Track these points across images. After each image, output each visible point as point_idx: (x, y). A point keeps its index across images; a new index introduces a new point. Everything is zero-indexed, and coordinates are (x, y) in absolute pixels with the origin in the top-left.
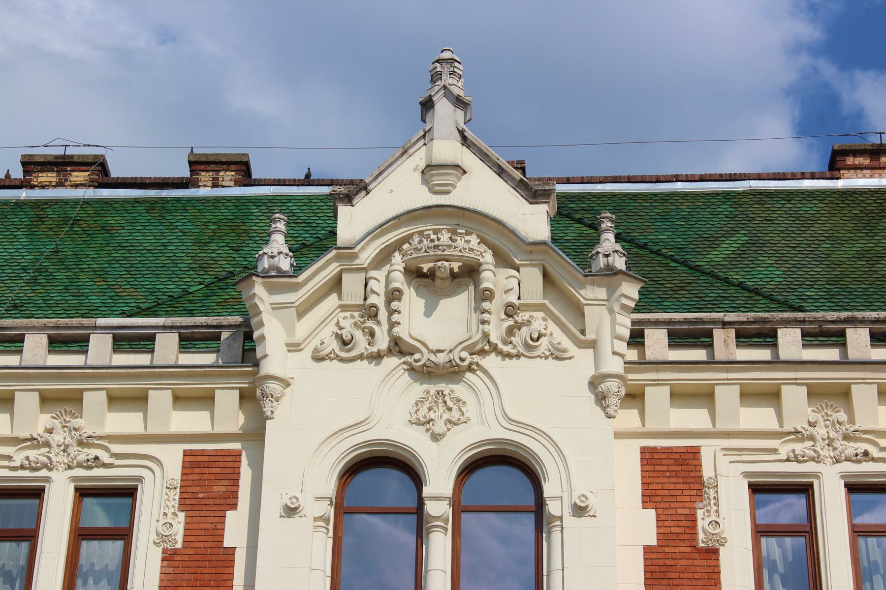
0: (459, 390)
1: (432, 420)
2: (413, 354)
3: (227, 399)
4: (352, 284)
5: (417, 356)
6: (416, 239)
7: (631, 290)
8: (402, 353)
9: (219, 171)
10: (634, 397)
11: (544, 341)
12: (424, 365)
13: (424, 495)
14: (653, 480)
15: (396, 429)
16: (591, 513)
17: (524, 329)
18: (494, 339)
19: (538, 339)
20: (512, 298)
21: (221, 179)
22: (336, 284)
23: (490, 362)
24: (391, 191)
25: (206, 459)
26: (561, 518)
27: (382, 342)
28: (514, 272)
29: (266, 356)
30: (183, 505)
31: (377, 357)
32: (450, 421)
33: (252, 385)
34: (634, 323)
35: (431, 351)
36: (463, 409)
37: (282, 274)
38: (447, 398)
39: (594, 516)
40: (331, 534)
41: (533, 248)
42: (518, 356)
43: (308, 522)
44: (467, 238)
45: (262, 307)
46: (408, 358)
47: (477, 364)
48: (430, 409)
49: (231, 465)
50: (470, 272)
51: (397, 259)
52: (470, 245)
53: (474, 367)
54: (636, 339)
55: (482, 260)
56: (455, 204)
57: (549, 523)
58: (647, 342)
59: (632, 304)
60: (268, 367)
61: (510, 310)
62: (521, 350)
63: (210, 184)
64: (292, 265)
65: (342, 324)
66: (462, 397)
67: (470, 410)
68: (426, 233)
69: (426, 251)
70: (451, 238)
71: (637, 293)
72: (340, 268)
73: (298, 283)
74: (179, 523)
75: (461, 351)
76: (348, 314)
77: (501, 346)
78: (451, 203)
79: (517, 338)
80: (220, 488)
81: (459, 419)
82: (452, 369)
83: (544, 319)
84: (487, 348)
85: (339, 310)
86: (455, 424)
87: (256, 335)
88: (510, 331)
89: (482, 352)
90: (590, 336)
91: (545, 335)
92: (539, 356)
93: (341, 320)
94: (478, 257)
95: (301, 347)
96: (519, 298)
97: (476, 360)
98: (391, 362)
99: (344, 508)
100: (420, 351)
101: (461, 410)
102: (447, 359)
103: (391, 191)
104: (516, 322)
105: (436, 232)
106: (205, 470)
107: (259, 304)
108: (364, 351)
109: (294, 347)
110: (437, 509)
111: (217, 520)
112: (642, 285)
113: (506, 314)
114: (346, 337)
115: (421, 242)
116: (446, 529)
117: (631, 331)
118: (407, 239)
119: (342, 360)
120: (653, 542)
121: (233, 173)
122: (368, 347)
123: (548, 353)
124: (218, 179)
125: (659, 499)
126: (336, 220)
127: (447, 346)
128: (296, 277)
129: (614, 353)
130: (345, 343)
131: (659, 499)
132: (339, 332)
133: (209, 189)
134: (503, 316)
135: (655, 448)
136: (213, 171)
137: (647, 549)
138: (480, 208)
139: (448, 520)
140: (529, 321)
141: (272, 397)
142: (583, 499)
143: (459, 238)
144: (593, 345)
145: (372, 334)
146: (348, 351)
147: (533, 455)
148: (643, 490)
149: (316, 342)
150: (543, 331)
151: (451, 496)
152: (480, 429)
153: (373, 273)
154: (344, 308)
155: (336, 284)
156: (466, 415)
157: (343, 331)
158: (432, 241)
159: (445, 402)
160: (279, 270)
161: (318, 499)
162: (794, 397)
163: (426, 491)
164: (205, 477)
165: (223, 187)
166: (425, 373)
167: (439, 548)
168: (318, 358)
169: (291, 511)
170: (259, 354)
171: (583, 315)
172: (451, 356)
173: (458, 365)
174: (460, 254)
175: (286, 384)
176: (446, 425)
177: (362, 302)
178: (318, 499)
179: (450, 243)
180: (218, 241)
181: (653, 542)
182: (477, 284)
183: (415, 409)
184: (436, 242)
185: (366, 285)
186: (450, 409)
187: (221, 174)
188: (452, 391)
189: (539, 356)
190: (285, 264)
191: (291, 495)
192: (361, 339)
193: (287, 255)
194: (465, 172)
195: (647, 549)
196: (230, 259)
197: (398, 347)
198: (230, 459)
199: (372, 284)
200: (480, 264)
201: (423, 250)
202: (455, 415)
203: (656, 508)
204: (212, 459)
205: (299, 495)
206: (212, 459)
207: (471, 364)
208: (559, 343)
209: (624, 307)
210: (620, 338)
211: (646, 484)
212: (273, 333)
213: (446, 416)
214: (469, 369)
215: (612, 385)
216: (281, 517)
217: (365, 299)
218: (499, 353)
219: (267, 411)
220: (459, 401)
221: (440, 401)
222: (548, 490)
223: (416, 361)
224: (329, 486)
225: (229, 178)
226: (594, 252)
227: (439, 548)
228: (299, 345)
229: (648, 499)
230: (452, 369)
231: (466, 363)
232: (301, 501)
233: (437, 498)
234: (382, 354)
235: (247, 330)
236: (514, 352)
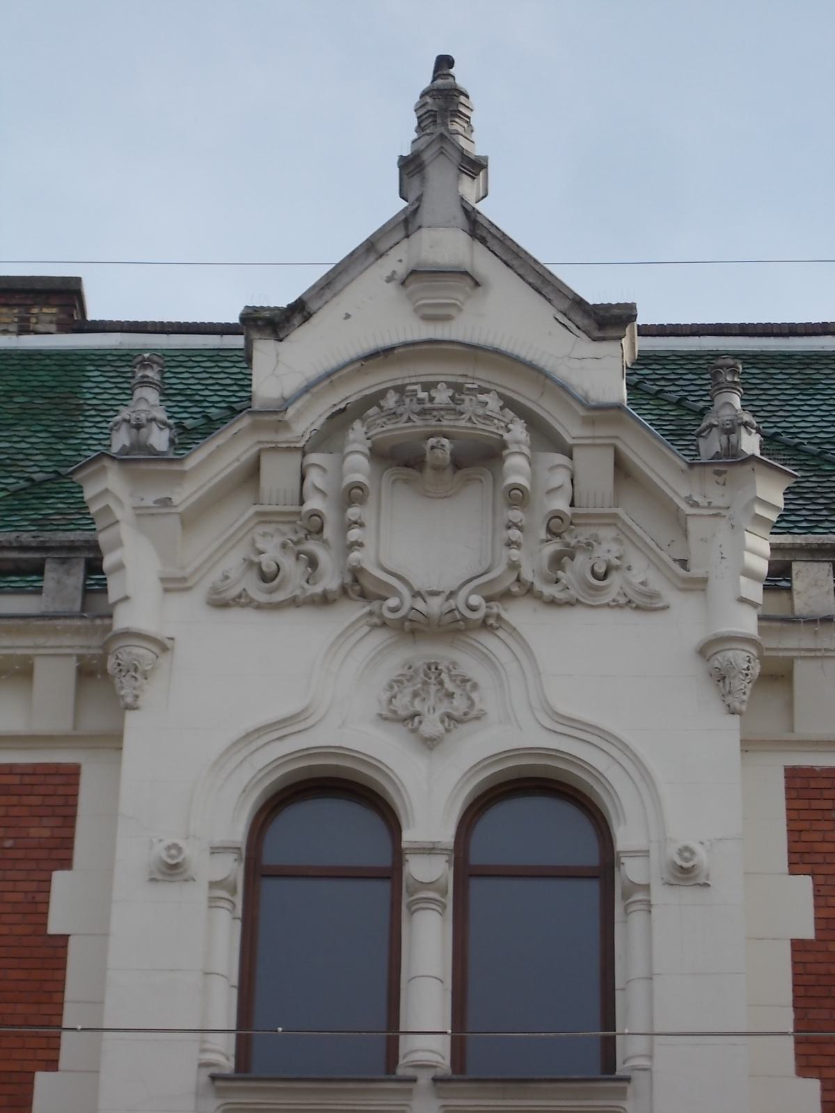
0: (468, 664)
1: (417, 714)
2: (386, 599)
3: (55, 676)
4: (278, 476)
5: (393, 602)
6: (391, 401)
7: (771, 492)
8: (364, 595)
9: (32, 306)
10: (777, 676)
11: (615, 579)
12: (404, 618)
13: (404, 845)
14: (805, 825)
15: (351, 728)
16: (701, 881)
17: (580, 558)
18: (527, 575)
19: (605, 576)
20: (560, 504)
21: (33, 320)
22: (253, 472)
23: (519, 614)
24: (348, 316)
25: (16, 780)
26: (646, 888)
27: (330, 581)
28: (561, 459)
29: (126, 599)
31: (325, 600)
32: (449, 716)
33: (100, 652)
34: (775, 548)
35: (416, 594)
36: (475, 696)
37: (156, 457)
38: (444, 676)
39: (707, 885)
40: (239, 912)
41: (597, 413)
42: (570, 604)
43: (198, 893)
44: (483, 398)
45: (119, 514)
46: (375, 606)
47: (499, 617)
48: (415, 695)
49: (61, 790)
50: (481, 457)
51: (357, 435)
52: (484, 415)
53: (491, 621)
54: (779, 577)
55: (506, 436)
56: (460, 339)
57: (626, 896)
58: (797, 584)
59: (774, 517)
60: (124, 619)
61: (556, 526)
62: (574, 593)
63: (13, 328)
64: (172, 442)
65: (260, 546)
66: (470, 675)
67: (487, 699)
68: (409, 388)
69: (409, 420)
70: (452, 398)
71: (782, 497)
72: (256, 449)
73: (185, 472)
75: (473, 592)
76: (269, 528)
77: (539, 586)
78: (453, 337)
79: (569, 574)
80: (39, 832)
81: (466, 714)
82: (454, 626)
83: (617, 540)
84: (515, 589)
85: (256, 520)
86: (459, 721)
87: (108, 563)
88: (557, 561)
89: (507, 595)
90: (696, 572)
91: (617, 568)
92: (608, 605)
93: (258, 539)
94: (500, 432)
95: (189, 584)
96: (572, 505)
97: (495, 610)
98: (354, 611)
99: (257, 869)
100: (396, 592)
101: (469, 698)
102: (446, 608)
103: (348, 316)
104: (568, 545)
105: (427, 387)
106: (15, 800)
107: (114, 507)
108: (298, 592)
109: (173, 585)
110: (429, 872)
111: (33, 886)
112: (790, 482)
113: (549, 530)
114: (269, 567)
115: (400, 402)
116: (444, 906)
117: (771, 564)
118: (374, 400)
119: (259, 607)
120: (808, 933)
121: (54, 310)
122: (306, 585)
123: (622, 600)
124: (28, 320)
125: (819, 858)
126: (250, 367)
127: (448, 584)
128: (180, 461)
129: (743, 600)
130: (265, 578)
131: (819, 858)
132: (256, 559)
133: (14, 337)
134: (543, 534)
135: (811, 770)
136: (18, 305)
137: (798, 947)
138: (504, 346)
139: (446, 892)
140: (589, 544)
141: (136, 670)
142: (687, 854)
143: (467, 398)
144: (699, 585)
145: (313, 563)
146: (271, 592)
147: (599, 776)
148: (791, 842)
149: (215, 576)
150: (616, 562)
151: (451, 846)
152: (510, 729)
153: (314, 458)
154: (264, 517)
155: (253, 472)
156: (478, 706)
157: (263, 558)
158: (421, 401)
159: (441, 683)
160: (150, 450)
161: (215, 850)
163: (409, 836)
164: (15, 811)
165: (37, 333)
166: (412, 628)
167: (428, 943)
168: (220, 603)
169: (172, 870)
170: (113, 594)
171: (685, 533)
172: (452, 603)
173: (465, 619)
174: (469, 425)
175: (163, 646)
176: (442, 722)
177: (295, 508)
178: (215, 850)
179: (453, 406)
180: (30, 422)
181: (808, 933)
182: (497, 476)
183: (388, 694)
184: (428, 405)
185: (303, 479)
186: (450, 695)
187: (35, 311)
188: (454, 664)
189: (608, 605)
190: (159, 439)
191: (168, 842)
192: (293, 569)
193: (165, 424)
194: (477, 284)
195: (798, 947)
196: (52, 452)
197: (358, 586)
198: (58, 780)
199: (314, 477)
200: (504, 445)
201: (405, 418)
202: (459, 704)
203: (813, 874)
204: (27, 780)
205: (181, 843)
206: (27, 780)
207: (487, 616)
208: (643, 583)
209: (759, 519)
210: (750, 574)
211: (794, 833)
212: (135, 562)
213: (444, 707)
214: (484, 625)
215: (739, 657)
216: (153, 880)
217: (302, 502)
218: (539, 597)
219: (127, 693)
220: (465, 681)
221: (433, 681)
222: (625, 838)
223: (394, 610)
224: (237, 832)
225: (48, 318)
226: (704, 424)
227: (428, 943)
228: (184, 579)
229: (799, 860)
230: (454, 626)
231: (478, 615)
232: (187, 851)
233: (430, 850)
234: (330, 597)
235: (91, 556)
236: (560, 596)
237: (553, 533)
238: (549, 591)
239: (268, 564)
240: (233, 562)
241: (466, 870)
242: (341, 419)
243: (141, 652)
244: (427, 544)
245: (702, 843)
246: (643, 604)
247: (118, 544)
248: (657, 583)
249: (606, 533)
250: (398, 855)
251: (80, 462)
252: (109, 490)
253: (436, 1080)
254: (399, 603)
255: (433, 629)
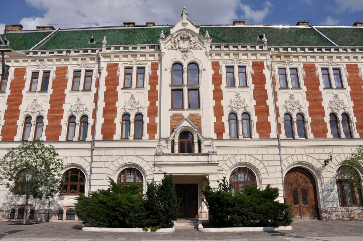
3: (156, 55)
4: (173, 39)
7: (210, 40)
8: (180, 49)
15: (179, 59)
22: (171, 40)
23: (192, 50)
27: (177, 48)
30: (56, 74)
31: (176, 49)
34: (211, 45)
37: (163, 38)
42: (195, 49)
52: (189, 34)
59: (211, 42)
67: (189, 57)
74: (13, 77)
80: (156, 67)
86: (187, 58)
88: (194, 46)
89: (191, 49)
98: (178, 50)
109: (165, 48)
110: (185, 70)
118: (180, 33)
137: (212, 75)
145: (176, 46)
154: (172, 43)
155: (171, 40)
162: (130, 56)
163: (184, 67)
166: (183, 52)
169: (166, 70)
170: (160, 49)
175: (164, 53)
195: (212, 75)
197: (179, 48)
202: (187, 57)
209: (210, 43)
210: (209, 47)
212: (162, 46)
214: (189, 51)
215: (208, 53)
224: (171, 67)
237: (194, 44)
238: (194, 48)
239: (172, 46)
240: (170, 46)
241: (188, 70)
242: (177, 36)
243: (163, 53)
244: (185, 45)
245: (355, 151)
246: (201, 49)
247: (161, 45)
248: (202, 47)
249: (198, 44)
250: (183, 69)
251: (52, 32)
252: (160, 41)
253: (186, 85)
254: (183, 50)
255: (185, 51)
